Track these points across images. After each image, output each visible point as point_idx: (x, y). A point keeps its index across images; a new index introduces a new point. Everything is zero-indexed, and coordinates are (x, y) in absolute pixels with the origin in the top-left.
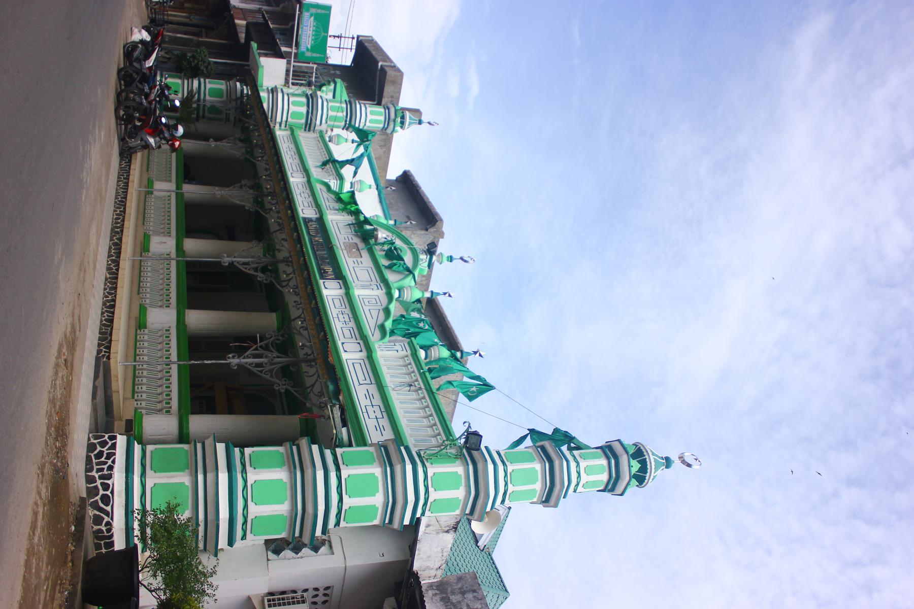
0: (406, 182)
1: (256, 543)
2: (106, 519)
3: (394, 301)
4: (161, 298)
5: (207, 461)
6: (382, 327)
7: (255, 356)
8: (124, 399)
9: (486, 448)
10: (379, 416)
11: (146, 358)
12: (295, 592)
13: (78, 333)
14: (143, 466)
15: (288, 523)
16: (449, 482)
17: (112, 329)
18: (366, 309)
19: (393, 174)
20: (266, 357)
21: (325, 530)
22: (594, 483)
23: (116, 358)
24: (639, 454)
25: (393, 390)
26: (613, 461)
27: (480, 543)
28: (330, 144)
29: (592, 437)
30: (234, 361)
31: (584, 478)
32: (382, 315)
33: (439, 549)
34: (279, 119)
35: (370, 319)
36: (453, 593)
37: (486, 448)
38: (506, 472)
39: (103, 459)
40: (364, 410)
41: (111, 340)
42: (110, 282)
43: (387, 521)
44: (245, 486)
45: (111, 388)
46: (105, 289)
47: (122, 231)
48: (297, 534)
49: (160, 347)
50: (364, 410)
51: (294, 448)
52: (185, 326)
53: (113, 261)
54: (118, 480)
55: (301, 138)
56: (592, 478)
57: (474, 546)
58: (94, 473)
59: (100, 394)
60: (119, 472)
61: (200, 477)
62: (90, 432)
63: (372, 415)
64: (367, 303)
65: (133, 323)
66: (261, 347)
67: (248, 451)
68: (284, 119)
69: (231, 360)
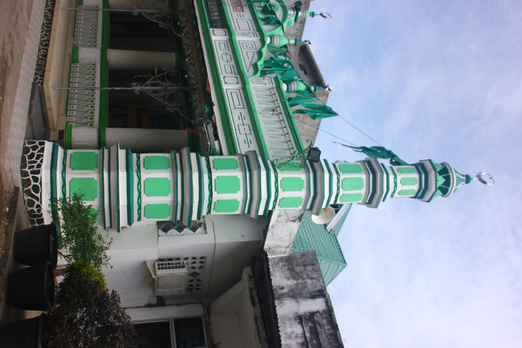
1: (151, 223)
2: (37, 203)
3: (266, 47)
4: (90, 40)
5: (111, 162)
6: (255, 66)
7: (153, 85)
8: (59, 115)
9: (325, 160)
11: (77, 85)
12: (178, 259)
13: (10, 64)
14: (64, 165)
15: (171, 211)
16: (294, 185)
17: (46, 62)
18: (244, 51)
20: (162, 86)
21: (199, 217)
22: (407, 192)
23: (48, 84)
24: (445, 171)
25: (260, 113)
26: (423, 176)
27: (328, 228)
29: (410, 155)
30: (137, 88)
31: (400, 187)
32: (256, 57)
33: (288, 233)
35: (246, 59)
36: (297, 265)
37: (325, 160)
38: (338, 180)
39: (34, 159)
40: (237, 128)
41: (45, 71)
42: (46, 27)
43: (246, 212)
44: (139, 182)
45: (46, 107)
46: (42, 32)
48: (178, 218)
49: (88, 77)
50: (237, 128)
51: (178, 155)
53: (49, 10)
54: (45, 175)
56: (406, 188)
57: (323, 229)
58: (27, 169)
59: (37, 111)
60: (45, 169)
61: (106, 175)
62: (26, 139)
63: (243, 132)
64: (245, 47)
65: (68, 59)
66: (158, 78)
67: (143, 156)
69: (135, 88)
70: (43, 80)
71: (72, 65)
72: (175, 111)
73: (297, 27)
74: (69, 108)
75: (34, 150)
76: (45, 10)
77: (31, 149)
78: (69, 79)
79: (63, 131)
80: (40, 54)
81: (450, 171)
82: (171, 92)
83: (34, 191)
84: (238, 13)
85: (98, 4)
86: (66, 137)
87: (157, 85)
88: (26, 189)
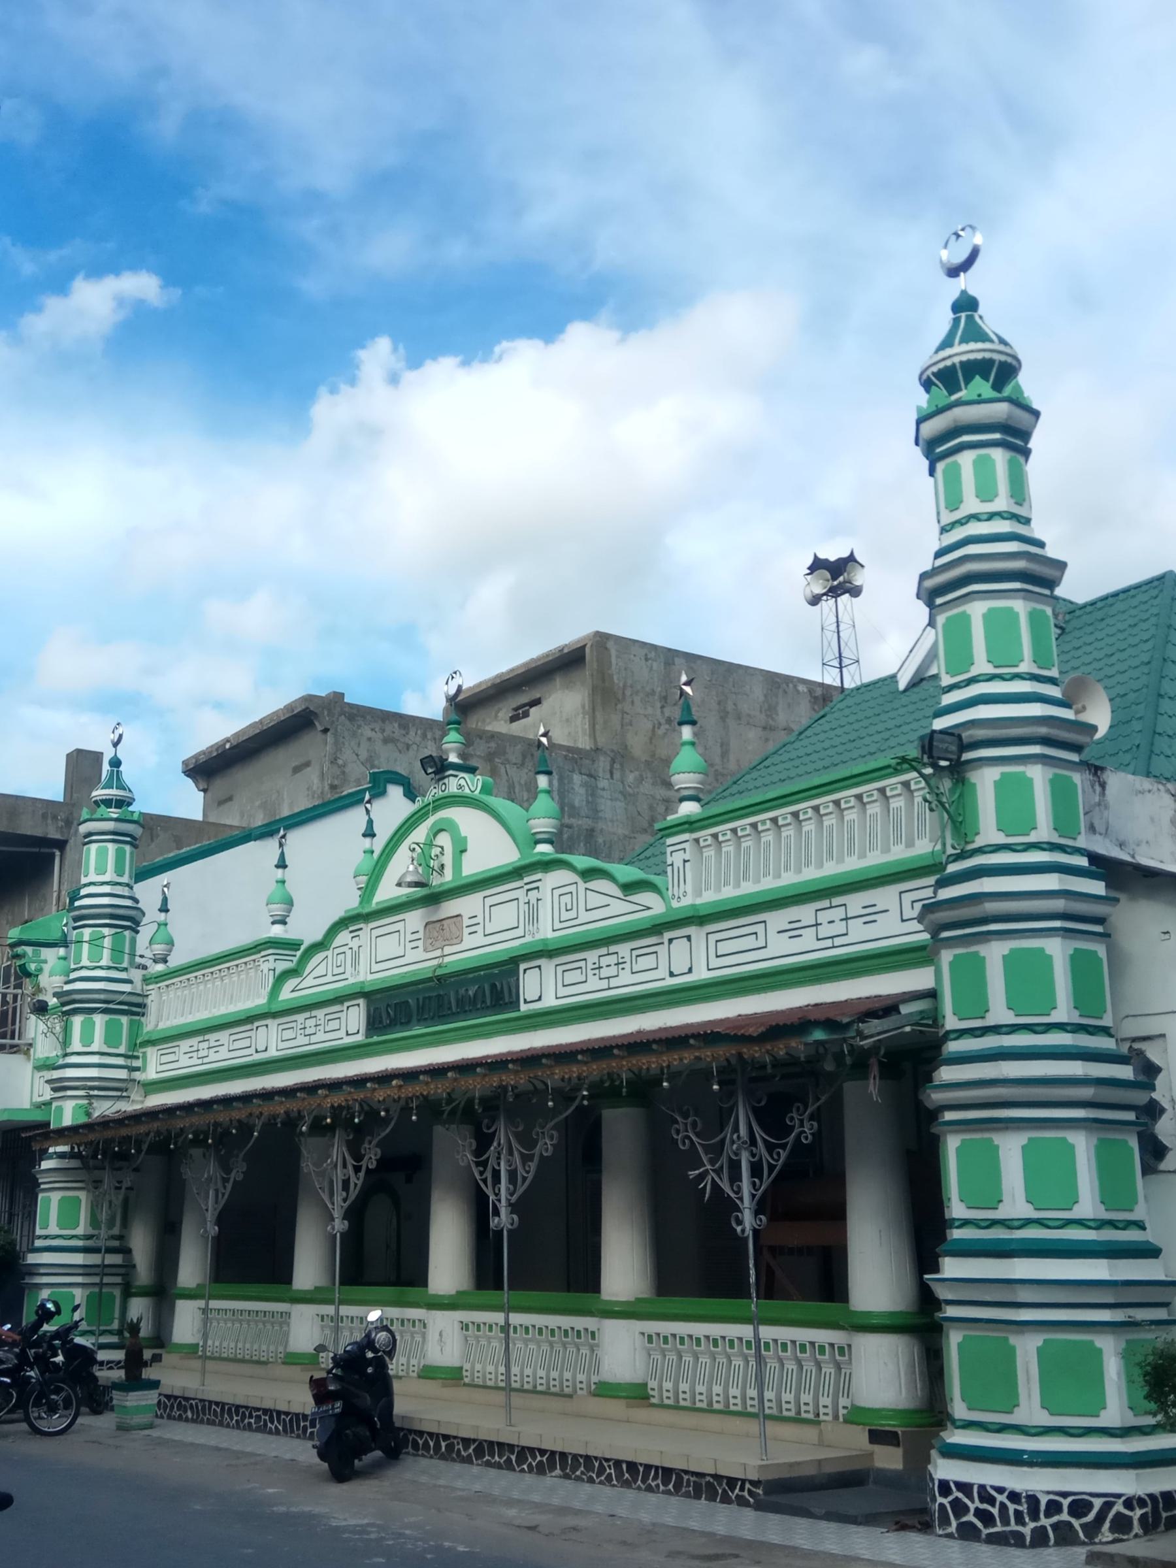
0: (208, 769)
2: (1119, 1507)
5: (988, 1298)
7: (735, 1177)
10: (839, 913)
11: (717, 1389)
14: (1002, 1428)
17: (686, 1472)
18: (585, 917)
19: (188, 803)
24: (945, 378)
28: (175, 961)
30: (748, 1221)
34: (122, 1074)
38: (992, 678)
39: (995, 1511)
40: (829, 943)
41: (716, 1477)
42: (574, 1470)
45: (812, 1476)
46: (591, 1481)
47: (446, 1437)
48: (1130, 1116)
49: (688, 1358)
50: (829, 943)
51: (949, 1116)
52: (638, 1300)
53: (521, 1458)
54: (1040, 1482)
55: (161, 1026)
63: (840, 927)
64: (572, 914)
67: (957, 1209)
68: (120, 1061)
70: (743, 1481)
71: (653, 1401)
72: (811, 1118)
73: (418, 739)
74: (792, 1414)
75: (967, 1509)
76: (523, 1471)
77: (964, 1519)
78: (668, 1407)
79: (870, 1431)
80: (662, 1488)
81: (948, 363)
82: (756, 1127)
83: (1086, 1515)
84: (466, 931)
85: (638, 1337)
86: (889, 1425)
87: (735, 1166)
88: (1081, 1535)
